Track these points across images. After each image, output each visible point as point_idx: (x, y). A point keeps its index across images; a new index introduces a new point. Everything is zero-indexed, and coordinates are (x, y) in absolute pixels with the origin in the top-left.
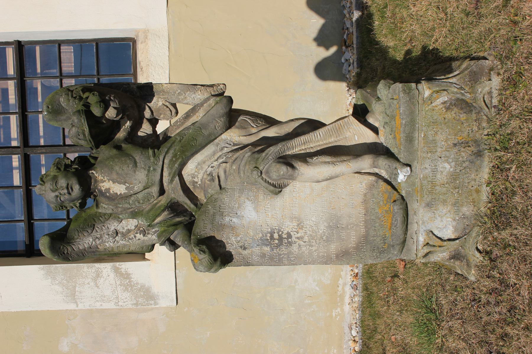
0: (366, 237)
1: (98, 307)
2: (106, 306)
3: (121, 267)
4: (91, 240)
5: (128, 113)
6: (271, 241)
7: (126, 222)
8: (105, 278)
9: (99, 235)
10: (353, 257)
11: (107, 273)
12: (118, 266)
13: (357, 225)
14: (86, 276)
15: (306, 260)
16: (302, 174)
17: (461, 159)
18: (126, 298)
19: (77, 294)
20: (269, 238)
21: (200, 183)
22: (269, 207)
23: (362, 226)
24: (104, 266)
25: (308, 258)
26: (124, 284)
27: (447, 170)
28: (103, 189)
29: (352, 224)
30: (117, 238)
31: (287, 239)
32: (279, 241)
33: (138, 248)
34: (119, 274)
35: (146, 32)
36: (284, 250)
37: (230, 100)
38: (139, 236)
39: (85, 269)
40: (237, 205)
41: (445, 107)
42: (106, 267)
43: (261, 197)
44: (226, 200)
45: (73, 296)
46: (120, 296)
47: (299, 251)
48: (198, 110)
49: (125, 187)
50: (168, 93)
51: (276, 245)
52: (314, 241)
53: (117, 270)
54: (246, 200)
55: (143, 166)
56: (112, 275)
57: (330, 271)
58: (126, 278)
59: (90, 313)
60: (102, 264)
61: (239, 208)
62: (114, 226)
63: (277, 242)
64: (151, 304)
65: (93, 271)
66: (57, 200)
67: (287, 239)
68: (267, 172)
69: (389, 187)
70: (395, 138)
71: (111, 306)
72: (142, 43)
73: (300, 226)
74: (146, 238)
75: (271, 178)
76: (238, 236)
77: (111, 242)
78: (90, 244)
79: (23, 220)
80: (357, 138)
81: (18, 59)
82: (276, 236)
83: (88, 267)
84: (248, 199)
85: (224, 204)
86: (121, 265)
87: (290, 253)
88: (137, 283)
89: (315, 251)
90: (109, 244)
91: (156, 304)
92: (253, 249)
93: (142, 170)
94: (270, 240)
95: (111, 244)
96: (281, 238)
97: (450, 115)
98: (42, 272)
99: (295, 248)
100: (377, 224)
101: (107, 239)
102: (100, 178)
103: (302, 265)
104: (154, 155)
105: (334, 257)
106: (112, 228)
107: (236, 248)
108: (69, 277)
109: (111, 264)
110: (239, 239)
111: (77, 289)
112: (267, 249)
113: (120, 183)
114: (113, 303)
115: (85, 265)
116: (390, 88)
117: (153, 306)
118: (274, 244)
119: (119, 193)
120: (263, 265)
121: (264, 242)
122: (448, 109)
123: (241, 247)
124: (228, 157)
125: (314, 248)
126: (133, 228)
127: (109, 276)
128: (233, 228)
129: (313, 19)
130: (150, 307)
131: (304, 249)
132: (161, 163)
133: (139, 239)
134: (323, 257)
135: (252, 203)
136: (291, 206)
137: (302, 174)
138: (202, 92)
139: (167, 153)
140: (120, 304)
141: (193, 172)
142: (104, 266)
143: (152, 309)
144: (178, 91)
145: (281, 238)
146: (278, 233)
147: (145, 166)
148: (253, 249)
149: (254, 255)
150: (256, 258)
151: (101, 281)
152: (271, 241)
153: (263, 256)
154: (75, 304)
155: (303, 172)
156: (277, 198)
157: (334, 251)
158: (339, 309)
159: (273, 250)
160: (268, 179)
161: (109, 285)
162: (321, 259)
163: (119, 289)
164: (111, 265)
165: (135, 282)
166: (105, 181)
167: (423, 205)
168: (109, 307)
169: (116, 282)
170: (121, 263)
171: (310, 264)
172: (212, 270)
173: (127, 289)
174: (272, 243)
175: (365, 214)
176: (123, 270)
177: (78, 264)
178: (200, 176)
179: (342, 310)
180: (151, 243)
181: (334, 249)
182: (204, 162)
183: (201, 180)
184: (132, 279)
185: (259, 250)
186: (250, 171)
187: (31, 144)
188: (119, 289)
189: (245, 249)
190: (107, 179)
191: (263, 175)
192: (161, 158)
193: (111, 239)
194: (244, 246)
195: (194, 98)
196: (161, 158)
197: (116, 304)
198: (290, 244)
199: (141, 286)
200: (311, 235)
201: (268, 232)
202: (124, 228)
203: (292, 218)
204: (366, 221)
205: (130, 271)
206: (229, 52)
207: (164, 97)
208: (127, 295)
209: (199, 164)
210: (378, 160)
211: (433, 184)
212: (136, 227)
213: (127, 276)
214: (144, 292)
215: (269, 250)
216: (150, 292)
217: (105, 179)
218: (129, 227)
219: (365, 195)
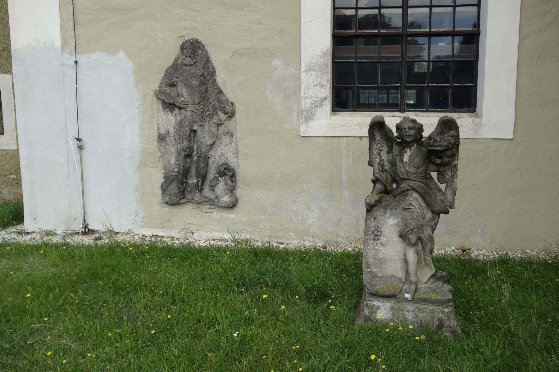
0: (376, 276)
1: (301, 85)
2: (302, 91)
4: (379, 139)
8: (321, 91)
13: (382, 272)
17: (414, 324)
18: (307, 104)
19: (311, 72)
21: (407, 198)
27: (409, 317)
28: (406, 149)
31: (377, 239)
35: (479, 116)
36: (372, 237)
37: (447, 212)
38: (378, 161)
39: (326, 78)
41: (439, 318)
43: (399, 228)
45: (310, 69)
46: (308, 100)
49: (407, 161)
50: (452, 182)
53: (325, 98)
54: (398, 221)
56: (322, 95)
57: (318, 232)
58: (319, 104)
59: (298, 80)
61: (394, 217)
63: (376, 234)
64: (302, 120)
66: (403, 128)
67: (377, 239)
68: (412, 233)
70: (425, 293)
71: (302, 94)
72: (472, 120)
73: (383, 245)
74: (376, 164)
76: (380, 216)
82: (379, 233)
83: (327, 80)
84: (399, 221)
87: (370, 239)
88: (316, 111)
91: (303, 123)
93: (415, 171)
96: (377, 236)
97: (436, 321)
98: (326, 50)
99: (372, 242)
100: (382, 282)
102: (412, 149)
104: (422, 177)
107: (375, 215)
110: (379, 216)
111: (314, 72)
112: (373, 229)
113: (409, 159)
114: (304, 95)
116: (449, 292)
117: (301, 121)
119: (404, 157)
121: (376, 228)
122: (438, 319)
125: (371, 251)
126: (383, 158)
128: (385, 214)
130: (301, 119)
131: (371, 246)
132: (419, 180)
133: (376, 161)
139: (423, 183)
140: (303, 100)
141: (413, 196)
143: (299, 120)
145: (377, 236)
146: (380, 235)
150: (369, 224)
151: (318, 88)
153: (370, 227)
154: (304, 71)
158: (294, 237)
159: (372, 232)
160: (408, 233)
163: (313, 99)
167: (393, 305)
168: (301, 93)
170: (329, 101)
172: (366, 205)
173: (313, 105)
176: (324, 103)
178: (410, 199)
179: (293, 239)
180: (373, 166)
182: (417, 201)
183: (408, 199)
186: (413, 224)
188: (313, 99)
189: (374, 219)
191: (410, 231)
192: (421, 180)
196: (421, 180)
197: (304, 98)
198: (374, 240)
199: (314, 114)
200: (378, 250)
201: (381, 230)
202: (382, 154)
203: (387, 241)
204: (383, 276)
205: (324, 107)
206: (463, 177)
208: (309, 105)
209: (417, 199)
211: (403, 310)
212: (383, 160)
213: (321, 105)
214: (310, 116)
216: (310, 119)
217: (412, 152)
219: (396, 276)
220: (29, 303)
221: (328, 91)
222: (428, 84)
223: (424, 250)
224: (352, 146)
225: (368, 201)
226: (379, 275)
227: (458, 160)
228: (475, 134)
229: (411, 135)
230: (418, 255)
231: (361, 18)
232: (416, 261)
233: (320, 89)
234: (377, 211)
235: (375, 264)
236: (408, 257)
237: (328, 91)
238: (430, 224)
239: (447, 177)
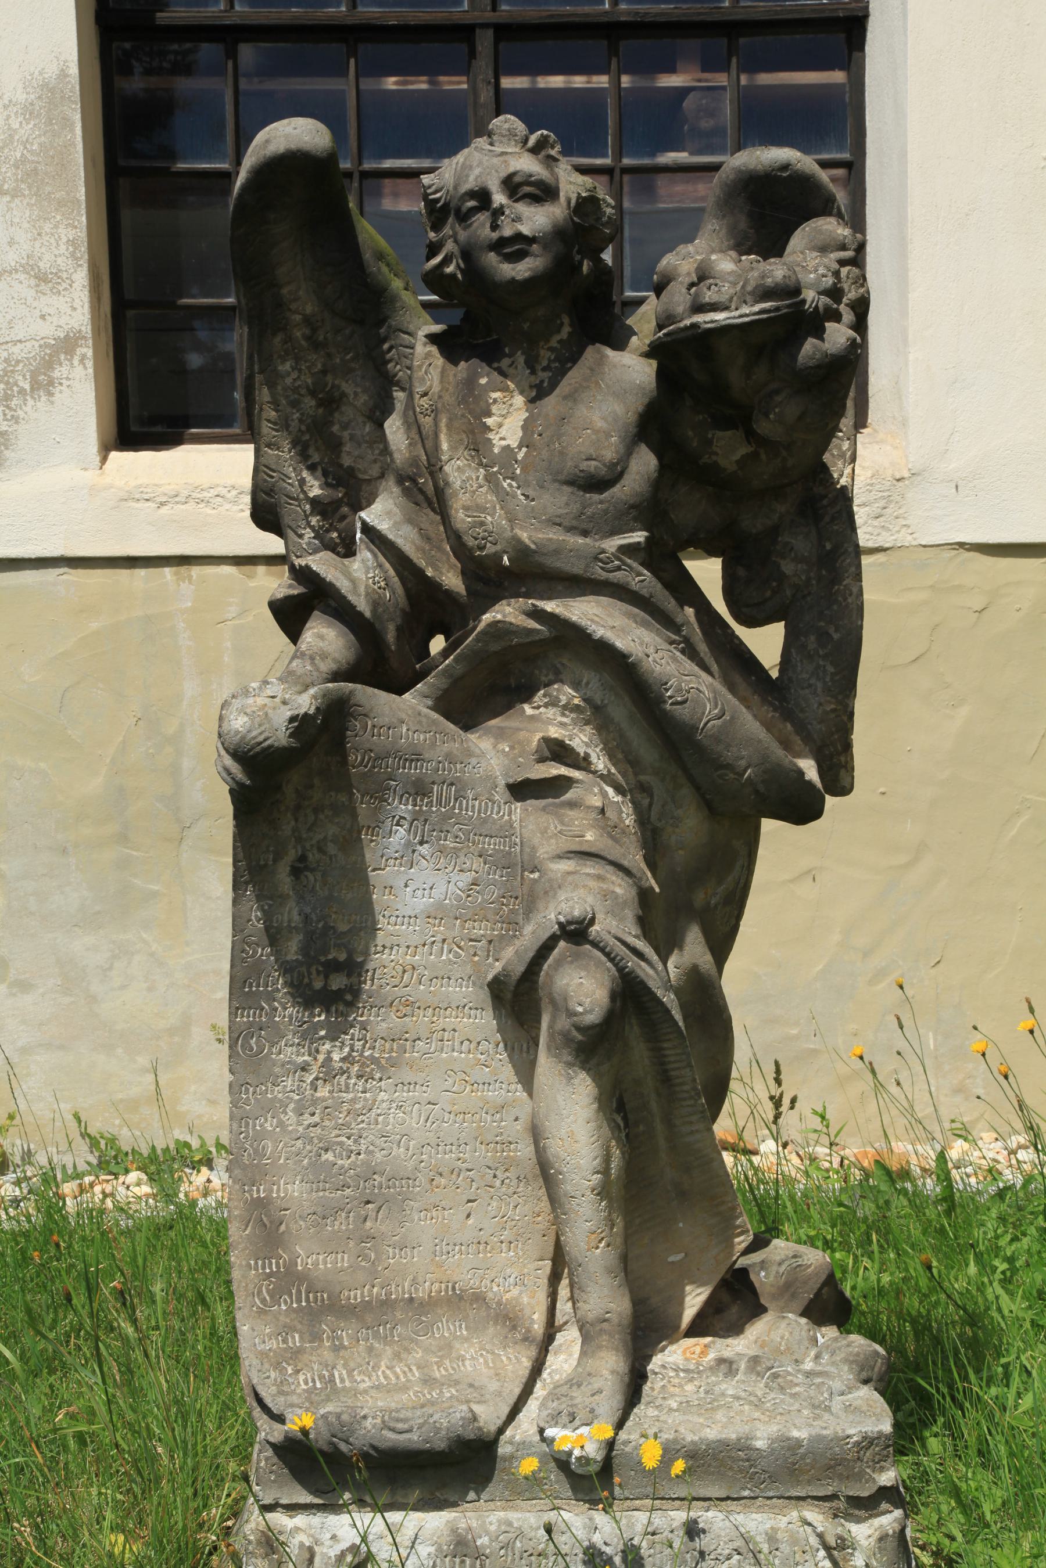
3: (76, 362)
4: (309, 309)
5: (763, 457)
6: (323, 964)
7: (367, 438)
8: (35, 304)
9: (325, 338)
10: (260, 1262)
11: (51, 311)
12: (78, 353)
13: (374, 1274)
14: (39, 234)
15: (247, 1090)
16: (570, 1078)
20: (330, 957)
22: (444, 957)
23: (370, 1295)
24: (77, 301)
25: (256, 1099)
26: (12, 372)
29: (377, 1258)
30: (309, 403)
32: (319, 991)
33: (272, 477)
34: (50, 355)
39: (66, 234)
40: (452, 845)
42: (74, 309)
44: (473, 806)
47: (283, 1065)
48: (771, 704)
49: (514, 444)
51: (306, 980)
52: (316, 1119)
53: (67, 345)
54: (468, 877)
55: (589, 511)
56: (48, 330)
60: (87, 293)
62: (356, 394)
63: (318, 985)
65: (59, 260)
69: (517, 1391)
75: (556, 970)
77: (295, 380)
78: (293, 306)
79: (232, 7)
80: (673, 1262)
81: (806, 16)
85: (456, 800)
86: (84, 364)
89: (281, 1124)
90: (288, 374)
92: (291, 903)
93: (575, 508)
94: (323, 959)
95: (288, 381)
99: (290, 1052)
101: (309, 368)
103: (228, 1077)
105: (258, 1191)
106: (347, 388)
107: (299, 840)
108: (36, 169)
109: (87, 330)
110: (332, 849)
115: (83, 234)
118: (310, 973)
119: (489, 421)
120: (234, 936)
123: (303, 858)
124: (622, 812)
126: (347, 461)
127: (43, 317)
129: (935, 1040)
134: (256, 1151)
135: (459, 899)
136: (443, 1036)
137: (570, 1078)
138: (832, 716)
142: (77, 301)
144: (836, 631)
147: (588, 517)
148: (291, 903)
149: (270, 906)
151: (23, 287)
152: (323, 964)
155: (576, 1081)
156: (474, 984)
157: (278, 1190)
161: (9, 317)
162: (251, 1146)
164: (83, 328)
165: (20, 413)
166: (533, 372)
169: (20, 341)
170: (90, 364)
171: (234, 1104)
172: (228, 761)
174: (314, 967)
175: (411, 1299)
177: (83, 206)
181: (286, 1191)
184: (30, 402)
185: (289, 921)
187: (502, 46)
189: (296, 872)
190: (542, 382)
193: (309, 381)
194: (307, 868)
195: (810, 686)
205: (61, 395)
207: (814, 582)
210: (617, 1350)
212: (351, 472)
215: (288, 958)
218: (347, 448)
220: (900, 1385)
221: (77, 303)
222: (619, 155)
223: (665, 1078)
224: (232, 611)
225: (238, 723)
226: (356, 1296)
227: (853, 460)
228: (876, 523)
229: (531, 240)
230: (625, 1119)
231: (516, 1074)
233: (33, 292)
234: (316, 811)
235: (326, 1213)
236: (555, 1147)
237: (77, 303)
238: (699, 898)
239: (788, 567)
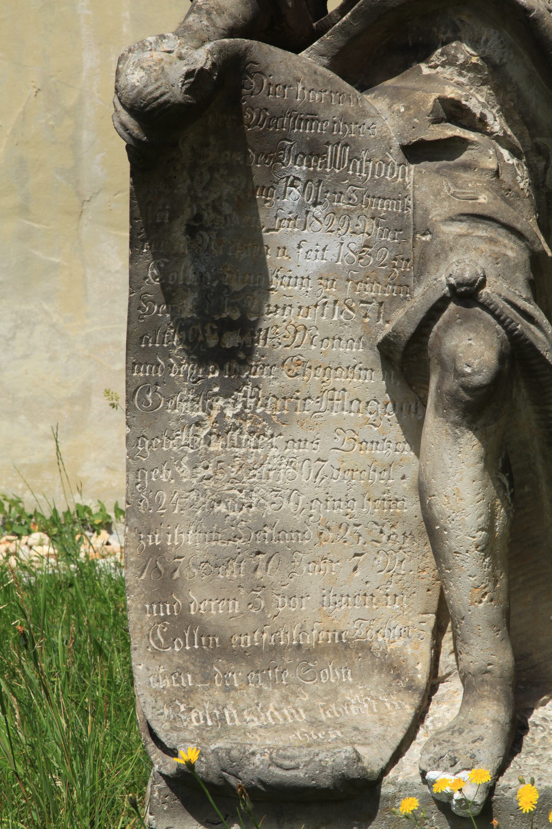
54: (361, 239)
63: (212, 342)
107: (195, 199)
110: (227, 209)
172: (125, 117)
230: (511, 479)
232: (430, 673)
234: (212, 169)
